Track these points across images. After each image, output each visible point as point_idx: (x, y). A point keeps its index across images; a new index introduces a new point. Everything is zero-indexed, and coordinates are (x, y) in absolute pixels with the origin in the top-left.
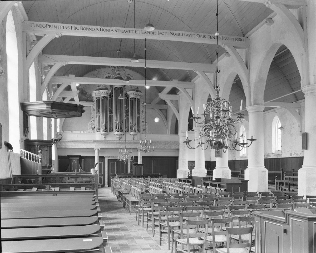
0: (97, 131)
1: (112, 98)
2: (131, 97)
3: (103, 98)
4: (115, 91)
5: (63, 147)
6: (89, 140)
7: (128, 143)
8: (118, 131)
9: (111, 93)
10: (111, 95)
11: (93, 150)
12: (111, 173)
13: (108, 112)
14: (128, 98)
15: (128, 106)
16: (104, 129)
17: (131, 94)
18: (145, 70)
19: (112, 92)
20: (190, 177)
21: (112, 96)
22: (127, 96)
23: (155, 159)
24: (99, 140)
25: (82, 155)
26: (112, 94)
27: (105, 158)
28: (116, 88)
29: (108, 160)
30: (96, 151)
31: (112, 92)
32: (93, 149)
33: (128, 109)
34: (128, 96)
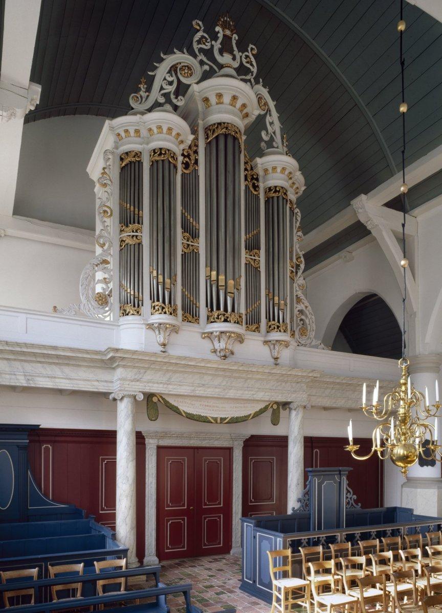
0: (125, 313)
1: (196, 171)
2: (272, 183)
3: (160, 154)
4: (209, 144)
5: (103, 581)
6: (87, 352)
7: (260, 379)
8: (226, 321)
9: (190, 147)
10: (188, 156)
11: (102, 400)
12: (168, 506)
13: (179, 230)
14: (256, 187)
15: (259, 226)
16: (164, 302)
17: (274, 168)
18: (403, 17)
19: (195, 144)
20: (39, 436)
21: (196, 162)
22: (252, 179)
23: (52, 442)
24: (135, 352)
25: (44, 425)
26: (196, 152)
27: (147, 441)
28: (220, 124)
29: (159, 448)
30: (124, 409)
31: (197, 146)
32: (106, 395)
33: (259, 233)
34: (257, 179)
